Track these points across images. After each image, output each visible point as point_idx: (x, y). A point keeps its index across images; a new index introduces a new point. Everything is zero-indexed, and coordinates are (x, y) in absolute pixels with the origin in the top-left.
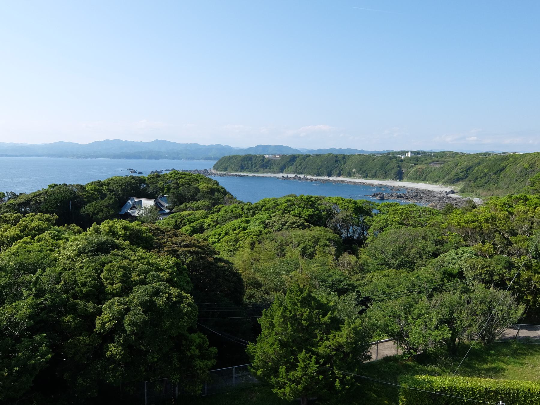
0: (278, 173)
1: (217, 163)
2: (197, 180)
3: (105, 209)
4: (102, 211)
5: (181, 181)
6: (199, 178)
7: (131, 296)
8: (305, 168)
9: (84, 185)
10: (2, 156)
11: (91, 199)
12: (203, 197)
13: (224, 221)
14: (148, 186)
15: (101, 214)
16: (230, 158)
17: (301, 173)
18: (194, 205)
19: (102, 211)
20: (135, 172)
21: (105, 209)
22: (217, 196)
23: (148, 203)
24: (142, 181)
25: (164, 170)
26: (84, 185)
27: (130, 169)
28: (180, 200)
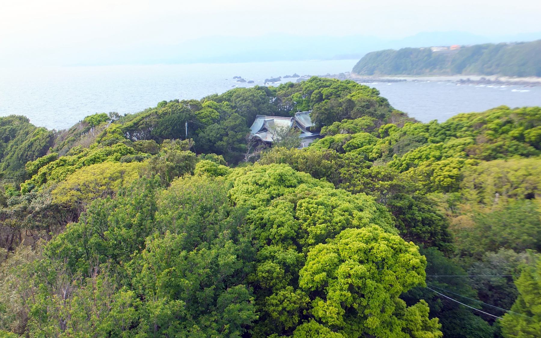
0: (453, 75)
1: (358, 64)
2: (347, 88)
3: (231, 133)
4: (227, 135)
5: (325, 91)
6: (349, 86)
7: (406, 243)
8: (498, 65)
9: (199, 100)
10: (538, 83)
11: (139, 122)
12: (361, 113)
13: (401, 150)
14: (278, 100)
15: (225, 138)
16: (379, 54)
17: (491, 74)
18: (347, 124)
19: (227, 135)
20: (243, 81)
21: (231, 133)
22: (378, 111)
23: (284, 123)
24: (269, 93)
25: (282, 76)
26: (199, 100)
27: (236, 77)
28: (326, 120)
